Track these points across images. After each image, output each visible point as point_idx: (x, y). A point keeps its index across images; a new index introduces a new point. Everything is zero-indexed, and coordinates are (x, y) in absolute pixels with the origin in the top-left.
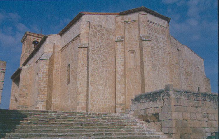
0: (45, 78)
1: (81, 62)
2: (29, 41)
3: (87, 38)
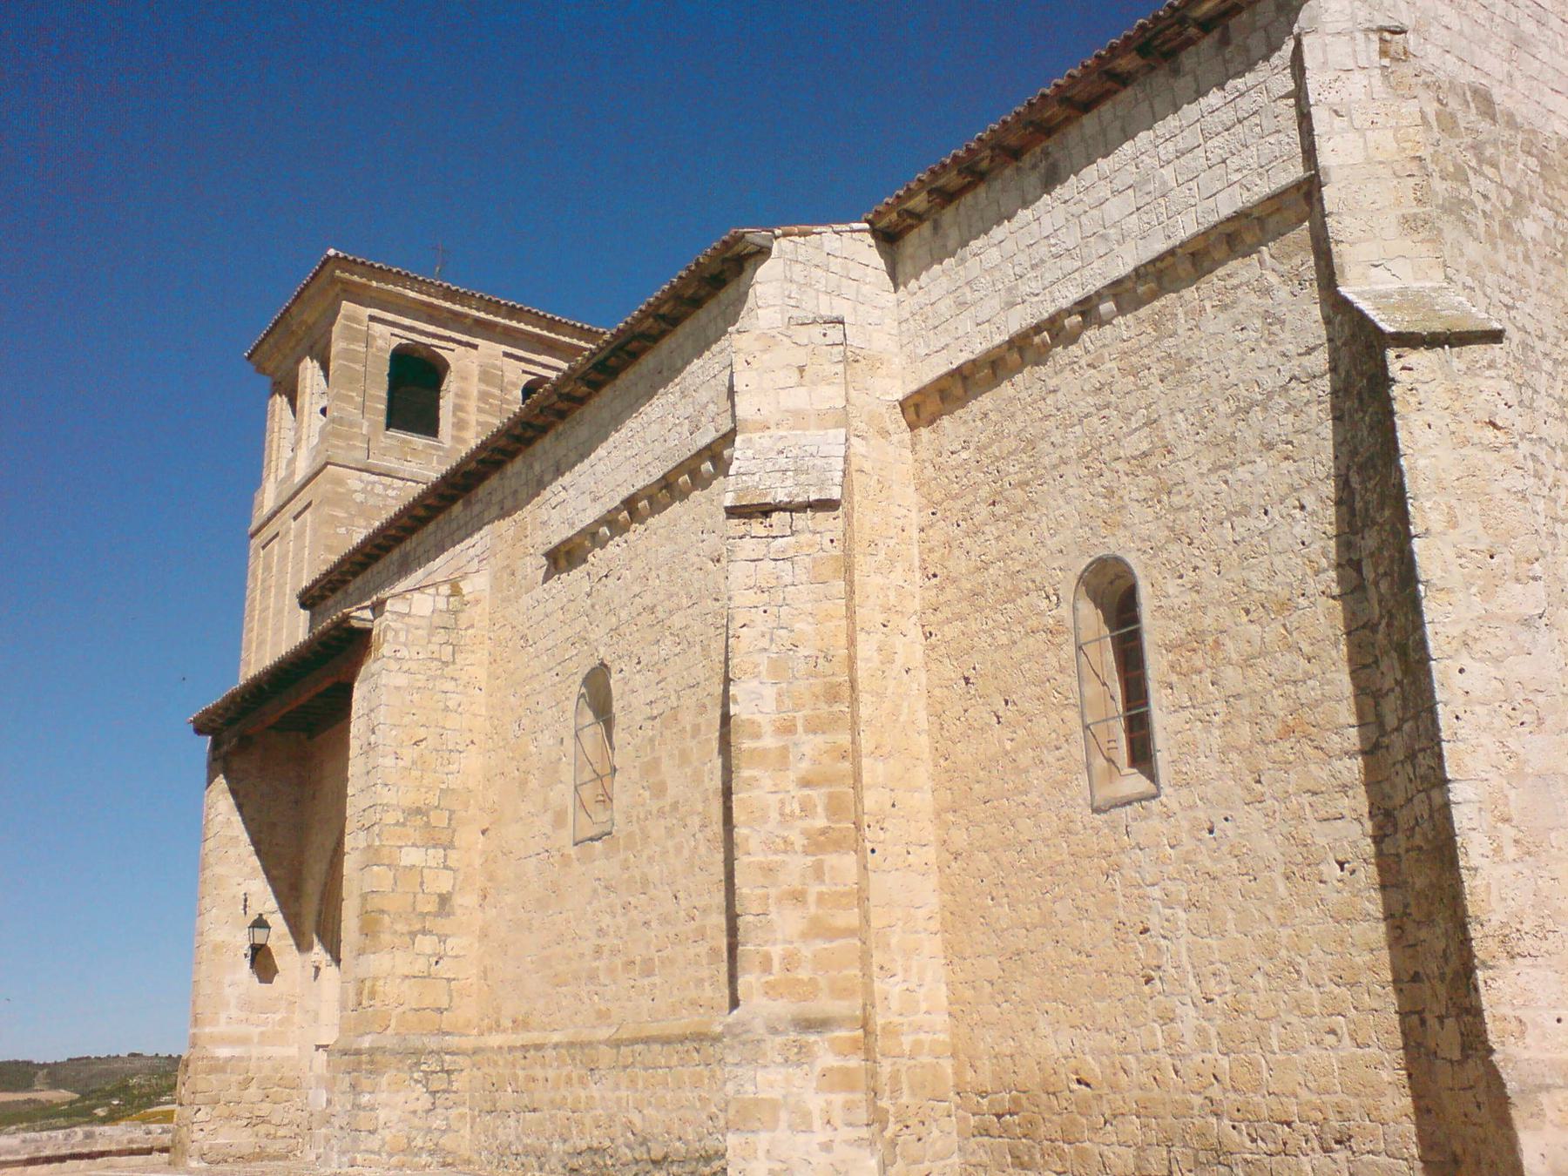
0: (813, 728)
1: (1453, 523)
2: (361, 348)
3: (1410, 224)
